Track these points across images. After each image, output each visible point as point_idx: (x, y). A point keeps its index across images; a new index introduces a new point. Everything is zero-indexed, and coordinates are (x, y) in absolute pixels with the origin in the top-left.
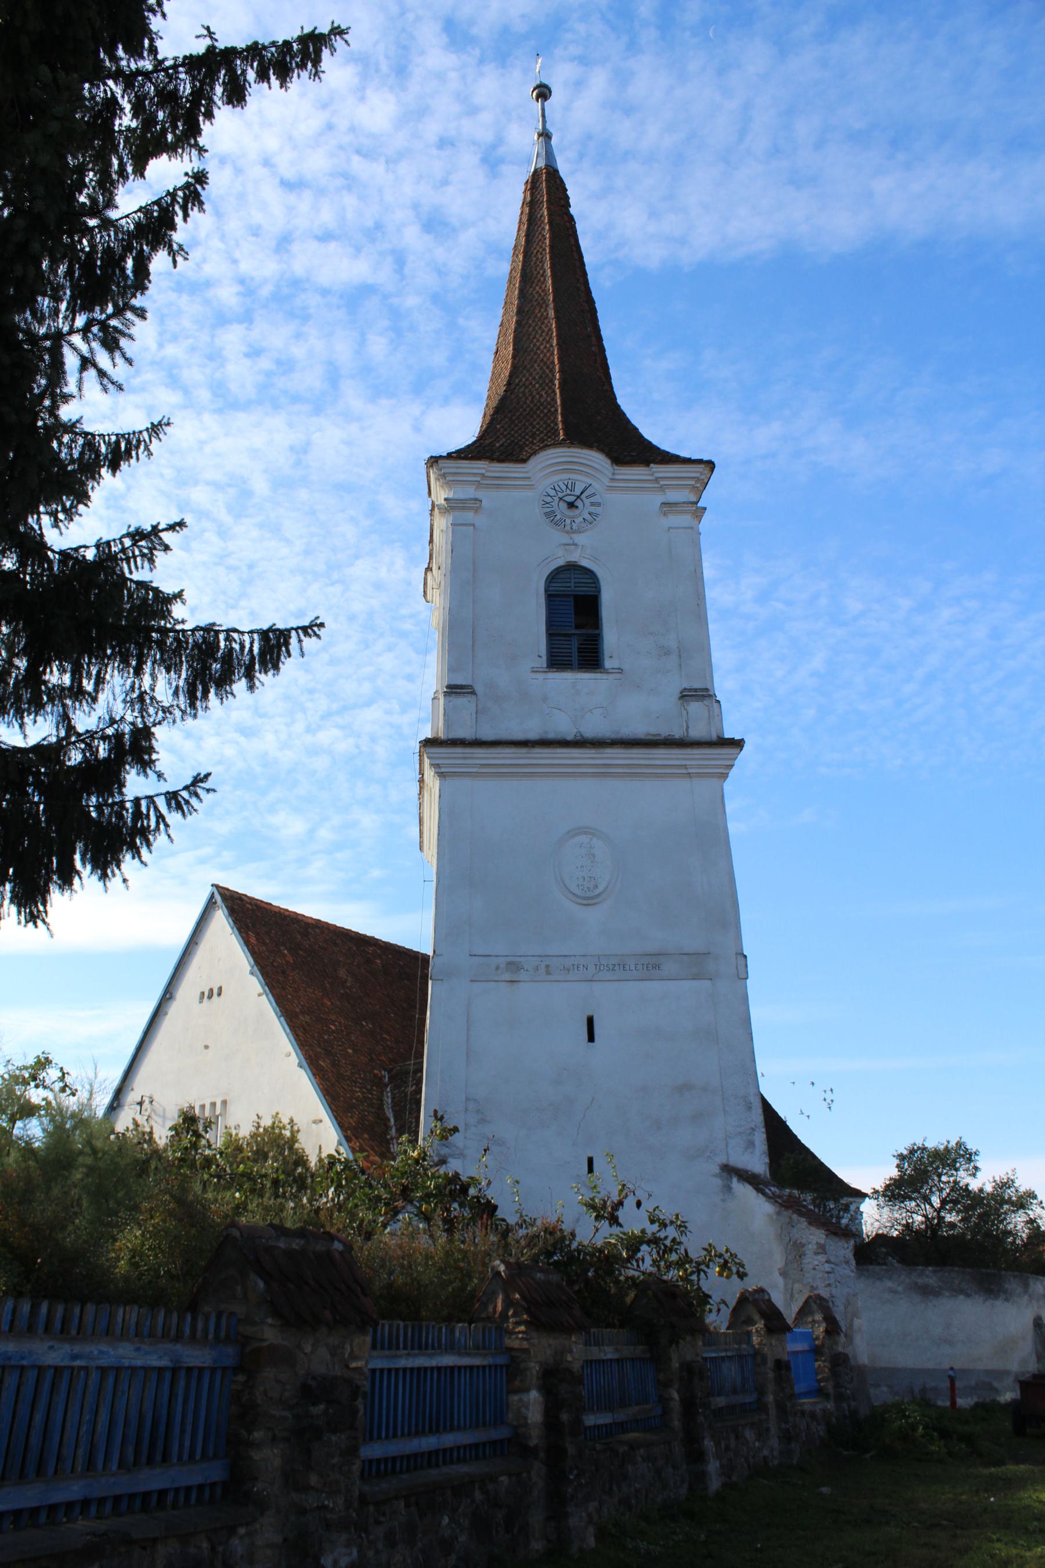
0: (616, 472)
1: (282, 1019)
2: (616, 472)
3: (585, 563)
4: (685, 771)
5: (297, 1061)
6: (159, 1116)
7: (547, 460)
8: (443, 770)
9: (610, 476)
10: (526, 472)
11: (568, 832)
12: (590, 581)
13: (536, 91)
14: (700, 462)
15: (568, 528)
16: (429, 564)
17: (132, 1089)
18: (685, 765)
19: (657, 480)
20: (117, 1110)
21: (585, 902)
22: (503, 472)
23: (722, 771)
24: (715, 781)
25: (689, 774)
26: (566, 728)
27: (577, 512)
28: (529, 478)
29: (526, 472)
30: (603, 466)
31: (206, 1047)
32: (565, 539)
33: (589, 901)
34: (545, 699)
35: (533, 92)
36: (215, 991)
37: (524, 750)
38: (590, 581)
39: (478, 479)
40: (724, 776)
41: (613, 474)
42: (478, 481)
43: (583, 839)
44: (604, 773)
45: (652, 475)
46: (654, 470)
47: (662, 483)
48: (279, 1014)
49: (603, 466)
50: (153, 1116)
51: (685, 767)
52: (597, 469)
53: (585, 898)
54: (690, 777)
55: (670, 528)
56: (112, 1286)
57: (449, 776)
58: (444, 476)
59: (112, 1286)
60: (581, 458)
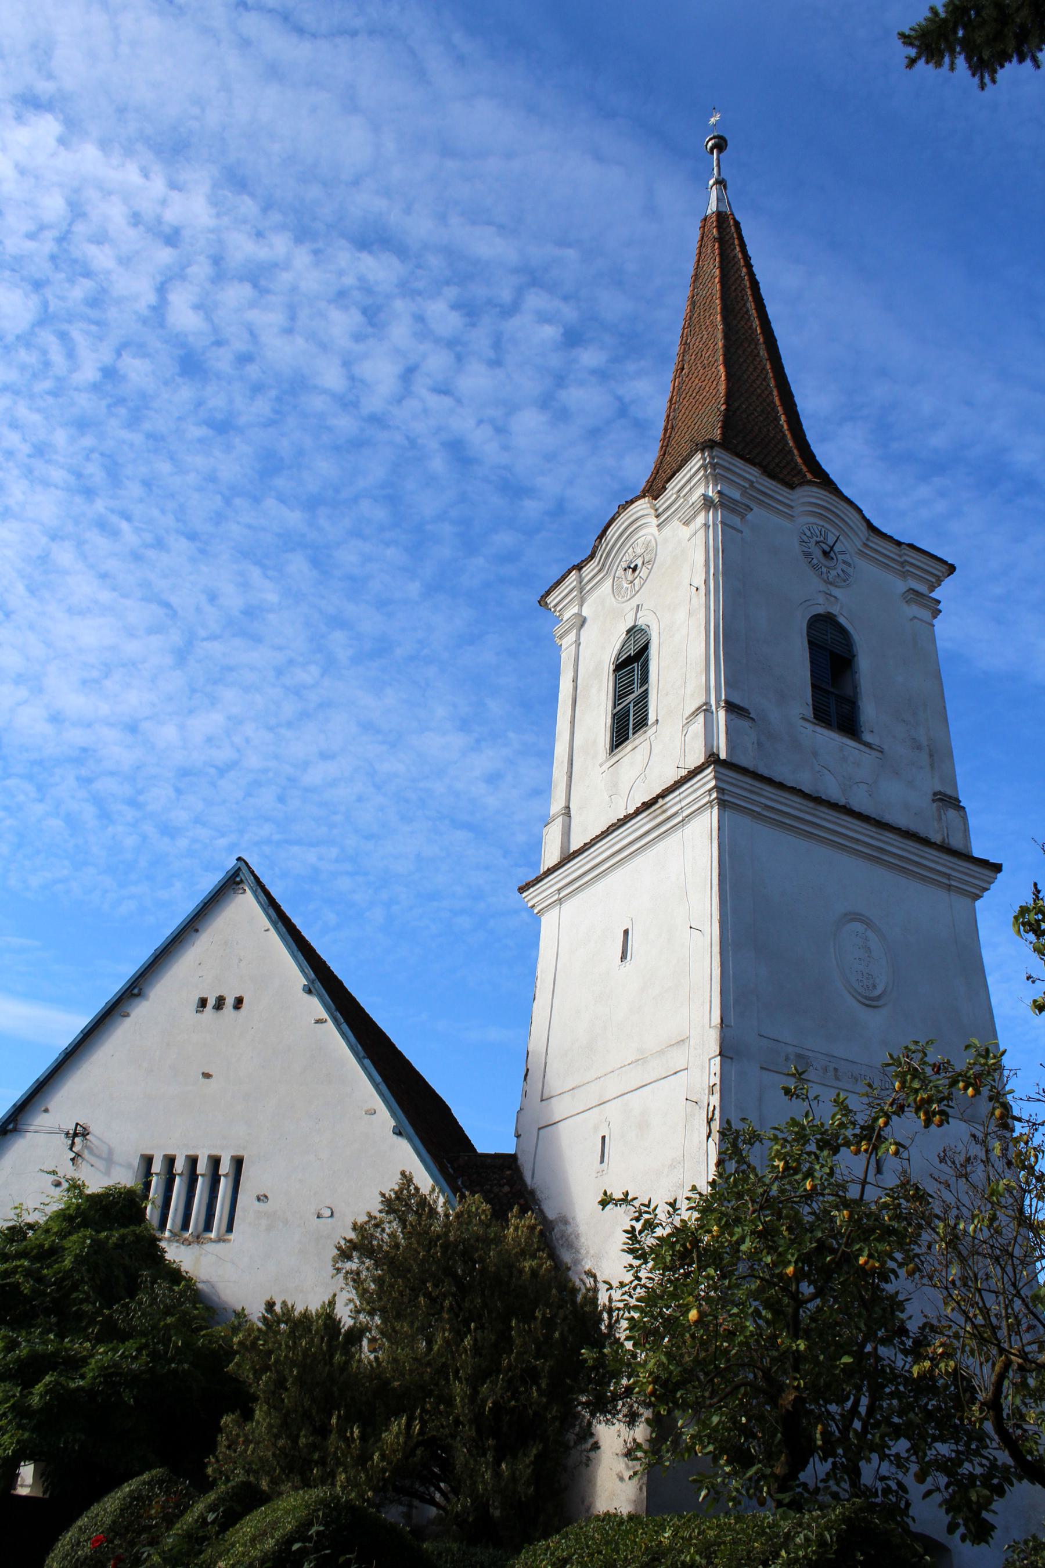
0: (871, 538)
1: (367, 1062)
2: (871, 538)
3: (842, 620)
4: (946, 881)
5: (393, 1123)
6: (99, 1157)
7: (810, 496)
8: (726, 798)
9: (864, 540)
10: (792, 500)
11: (846, 915)
12: (843, 642)
13: (716, 140)
14: (945, 562)
15: (825, 576)
16: (583, 561)
17: (46, 1111)
18: (949, 875)
19: (903, 564)
20: (9, 1136)
21: (867, 1002)
22: (773, 490)
23: (977, 892)
24: (969, 900)
25: (950, 886)
26: (833, 791)
27: (832, 564)
28: (792, 507)
29: (792, 500)
30: (858, 527)
31: (207, 1076)
32: (823, 587)
33: (871, 1003)
34: (815, 754)
35: (710, 140)
36: (230, 1001)
37: (811, 804)
38: (843, 642)
39: (747, 485)
40: (978, 897)
41: (868, 539)
42: (746, 488)
43: (859, 927)
44: (876, 858)
45: (900, 556)
46: (904, 551)
47: (908, 568)
48: (362, 1053)
49: (858, 527)
50: (86, 1154)
51: (948, 876)
52: (852, 528)
53: (866, 998)
54: (949, 890)
55: (915, 618)
56: (281, 1443)
57: (730, 807)
58: (714, 466)
59: (281, 1443)
60: (839, 509)
